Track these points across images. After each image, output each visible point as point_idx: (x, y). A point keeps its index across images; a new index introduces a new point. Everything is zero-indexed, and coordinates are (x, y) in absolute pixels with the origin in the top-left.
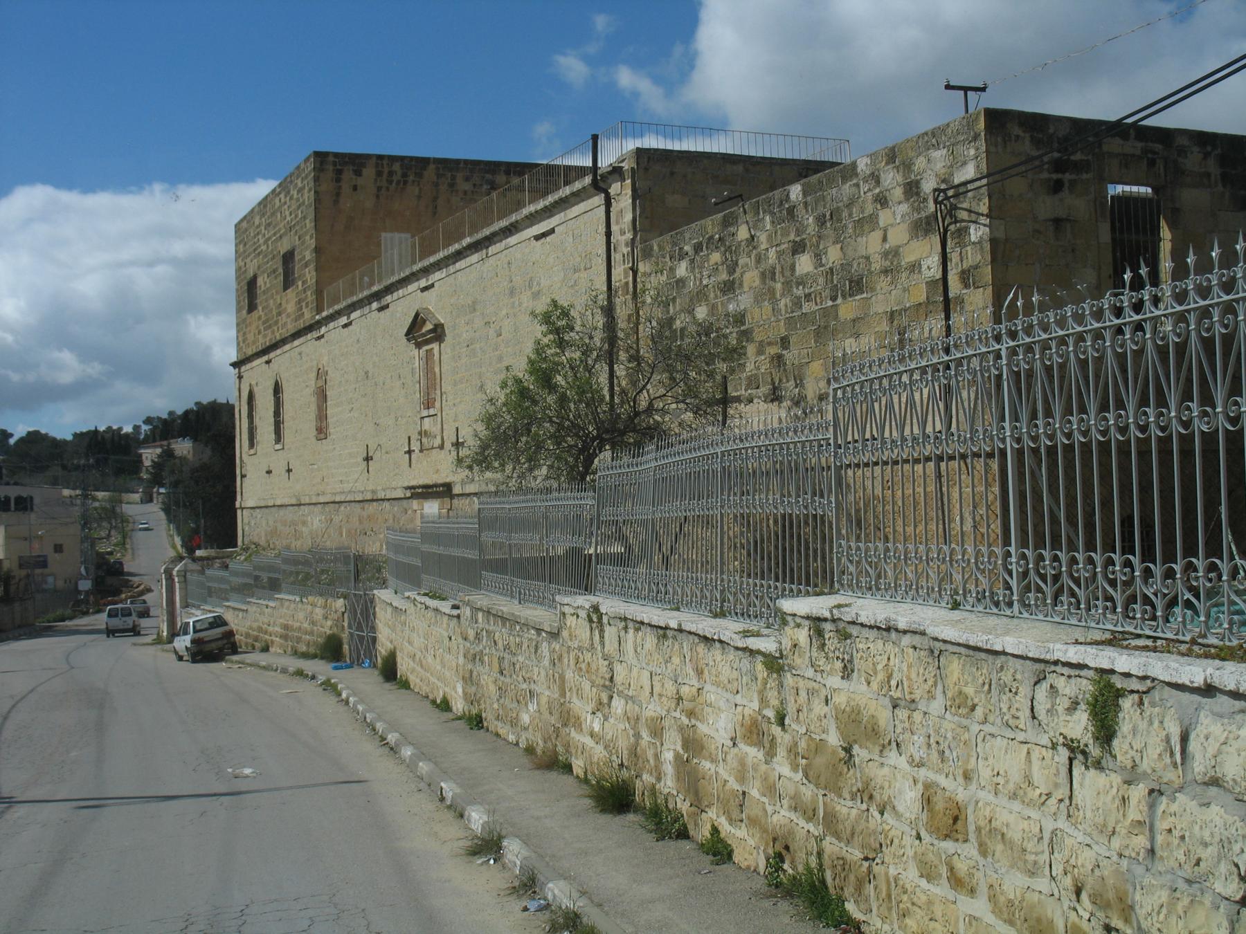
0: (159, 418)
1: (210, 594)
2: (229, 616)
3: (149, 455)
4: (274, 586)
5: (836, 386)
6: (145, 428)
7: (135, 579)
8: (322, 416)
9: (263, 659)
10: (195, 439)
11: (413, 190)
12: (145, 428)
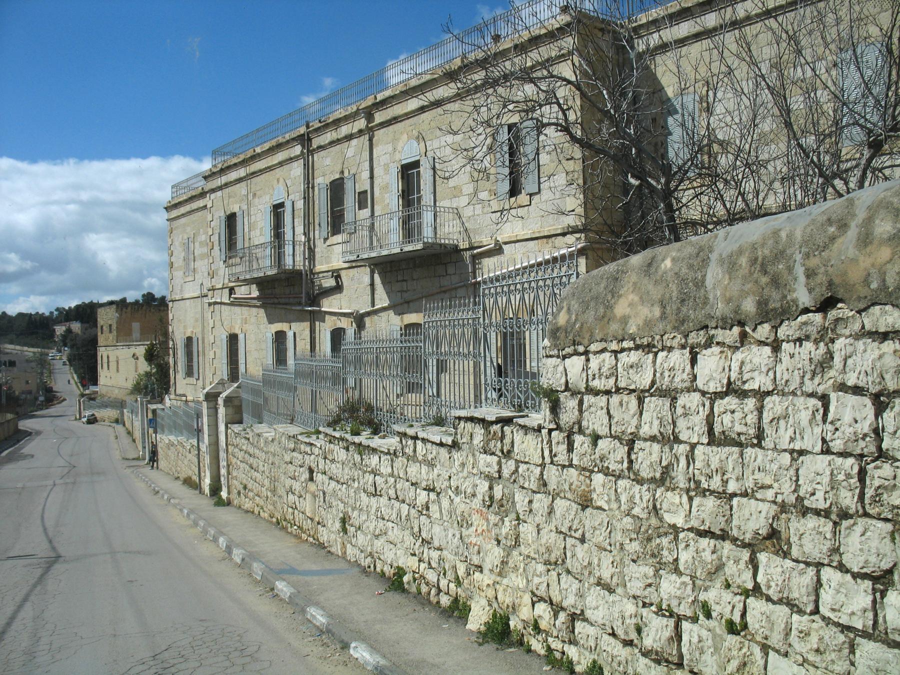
0: (64, 309)
1: (91, 407)
2: (95, 413)
3: (60, 330)
4: (106, 407)
5: (485, 287)
6: (56, 313)
7: (58, 394)
8: (118, 367)
9: (103, 423)
10: (82, 322)
11: (140, 312)
12: (56, 313)
